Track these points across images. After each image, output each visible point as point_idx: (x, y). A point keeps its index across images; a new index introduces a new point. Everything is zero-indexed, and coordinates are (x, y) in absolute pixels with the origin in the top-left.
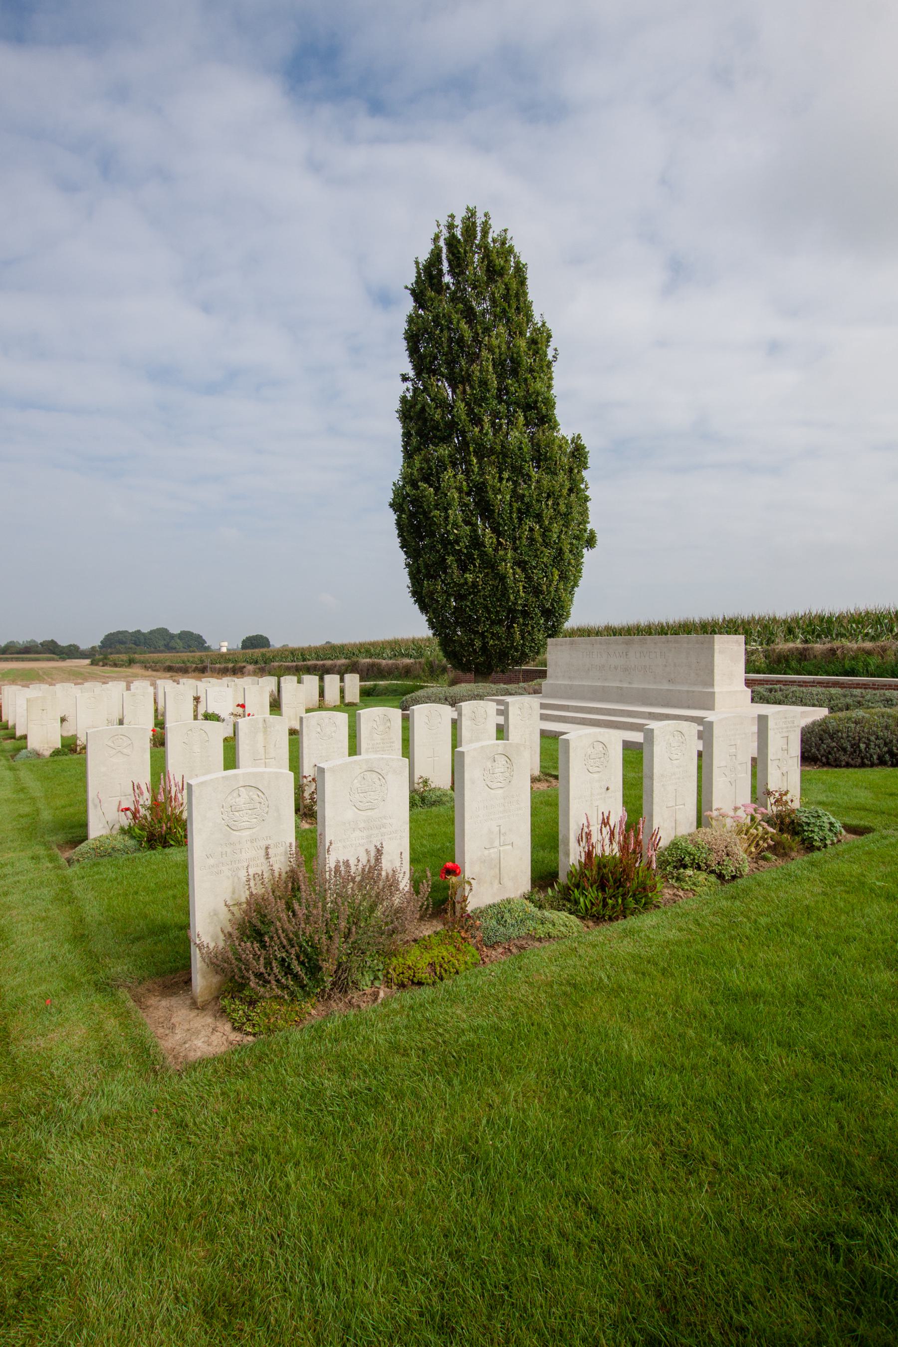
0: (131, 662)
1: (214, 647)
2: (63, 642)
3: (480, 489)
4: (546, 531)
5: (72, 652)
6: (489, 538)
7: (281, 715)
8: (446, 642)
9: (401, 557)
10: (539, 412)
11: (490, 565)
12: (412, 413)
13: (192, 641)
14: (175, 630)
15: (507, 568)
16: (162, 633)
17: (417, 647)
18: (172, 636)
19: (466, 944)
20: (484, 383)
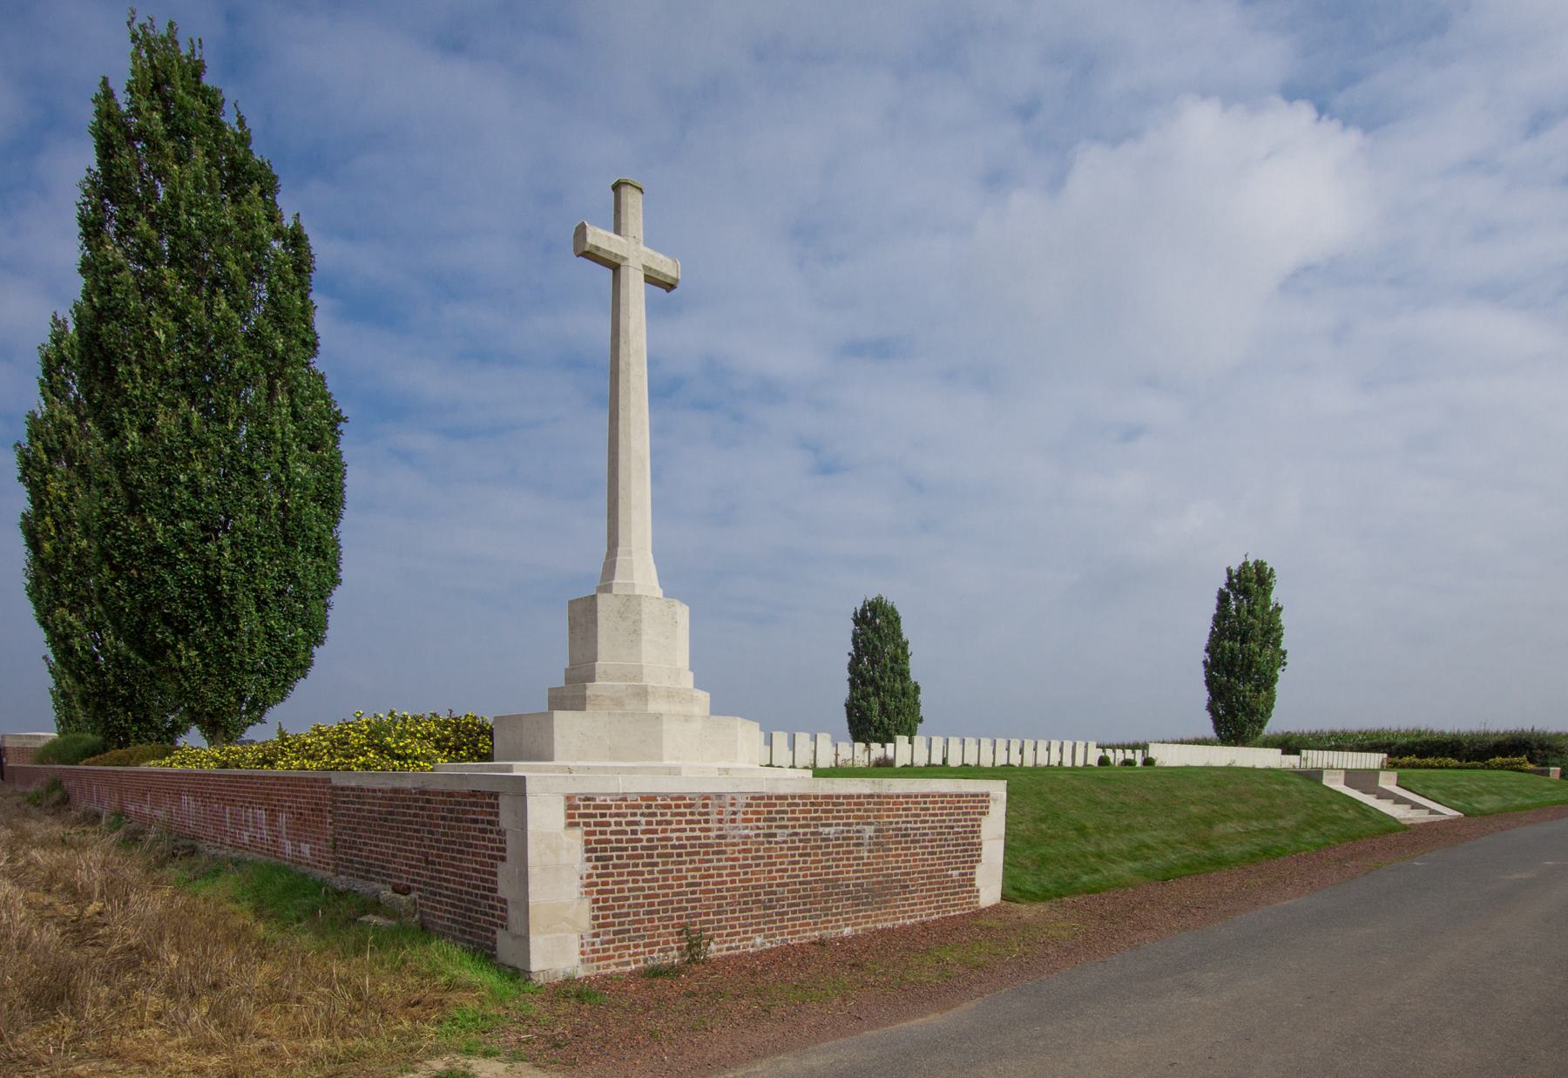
10: (904, 675)
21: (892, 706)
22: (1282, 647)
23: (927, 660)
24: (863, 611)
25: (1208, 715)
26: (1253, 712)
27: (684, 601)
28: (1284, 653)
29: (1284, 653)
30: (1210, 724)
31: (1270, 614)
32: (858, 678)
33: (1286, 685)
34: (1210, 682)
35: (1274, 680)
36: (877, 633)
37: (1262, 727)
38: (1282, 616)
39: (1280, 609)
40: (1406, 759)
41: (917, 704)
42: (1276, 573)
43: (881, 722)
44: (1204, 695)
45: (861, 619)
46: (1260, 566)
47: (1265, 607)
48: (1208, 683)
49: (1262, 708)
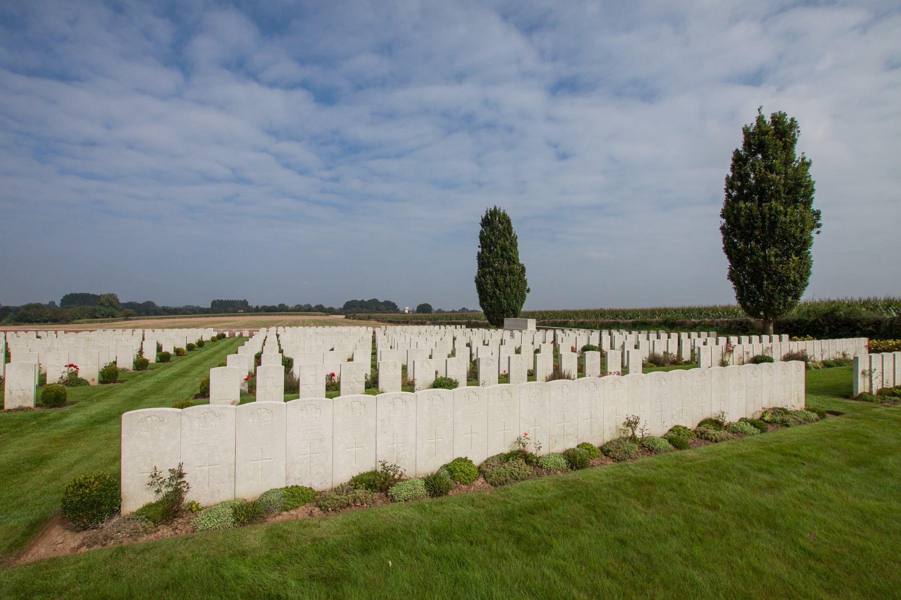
0: (369, 318)
1: (401, 309)
2: (326, 306)
3: (496, 280)
4: (512, 290)
5: (331, 311)
6: (498, 292)
7: (478, 385)
8: (487, 313)
9: (477, 294)
10: (513, 260)
11: (498, 299)
12: (480, 257)
13: (390, 307)
14: (381, 300)
15: (502, 300)
16: (375, 301)
17: (727, 310)
18: (380, 303)
19: (656, 532)
20: (497, 253)
21: (501, 280)
22: (814, 207)
23: (528, 253)
24: (487, 217)
25: (730, 285)
26: (783, 281)
27: (785, 333)
28: (817, 214)
29: (817, 214)
30: (734, 294)
31: (796, 170)
32: (483, 262)
33: (822, 248)
34: (730, 249)
35: (806, 243)
36: (496, 235)
37: (796, 297)
38: (811, 170)
39: (809, 164)
40: (286, 147)
41: (525, 282)
42: (800, 124)
43: (495, 293)
44: (725, 264)
45: (487, 222)
46: (778, 120)
47: (788, 161)
48: (727, 250)
49: (793, 275)
